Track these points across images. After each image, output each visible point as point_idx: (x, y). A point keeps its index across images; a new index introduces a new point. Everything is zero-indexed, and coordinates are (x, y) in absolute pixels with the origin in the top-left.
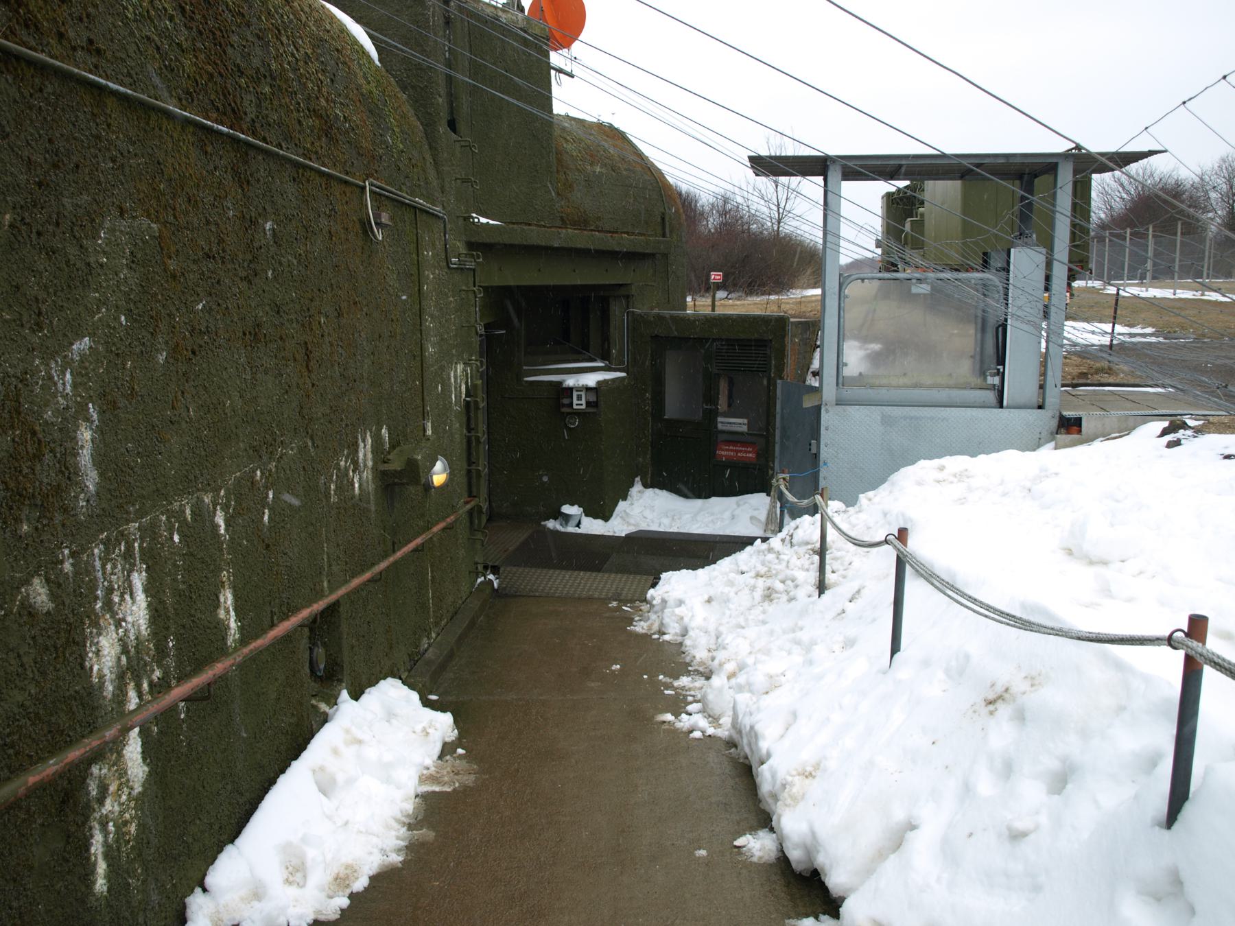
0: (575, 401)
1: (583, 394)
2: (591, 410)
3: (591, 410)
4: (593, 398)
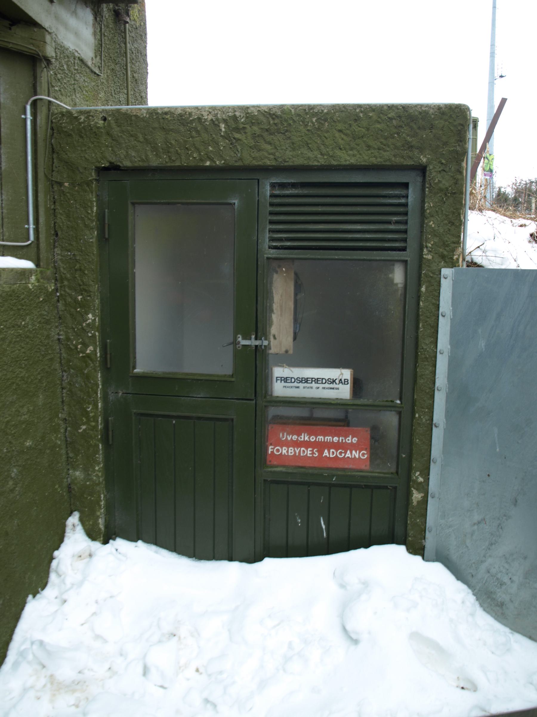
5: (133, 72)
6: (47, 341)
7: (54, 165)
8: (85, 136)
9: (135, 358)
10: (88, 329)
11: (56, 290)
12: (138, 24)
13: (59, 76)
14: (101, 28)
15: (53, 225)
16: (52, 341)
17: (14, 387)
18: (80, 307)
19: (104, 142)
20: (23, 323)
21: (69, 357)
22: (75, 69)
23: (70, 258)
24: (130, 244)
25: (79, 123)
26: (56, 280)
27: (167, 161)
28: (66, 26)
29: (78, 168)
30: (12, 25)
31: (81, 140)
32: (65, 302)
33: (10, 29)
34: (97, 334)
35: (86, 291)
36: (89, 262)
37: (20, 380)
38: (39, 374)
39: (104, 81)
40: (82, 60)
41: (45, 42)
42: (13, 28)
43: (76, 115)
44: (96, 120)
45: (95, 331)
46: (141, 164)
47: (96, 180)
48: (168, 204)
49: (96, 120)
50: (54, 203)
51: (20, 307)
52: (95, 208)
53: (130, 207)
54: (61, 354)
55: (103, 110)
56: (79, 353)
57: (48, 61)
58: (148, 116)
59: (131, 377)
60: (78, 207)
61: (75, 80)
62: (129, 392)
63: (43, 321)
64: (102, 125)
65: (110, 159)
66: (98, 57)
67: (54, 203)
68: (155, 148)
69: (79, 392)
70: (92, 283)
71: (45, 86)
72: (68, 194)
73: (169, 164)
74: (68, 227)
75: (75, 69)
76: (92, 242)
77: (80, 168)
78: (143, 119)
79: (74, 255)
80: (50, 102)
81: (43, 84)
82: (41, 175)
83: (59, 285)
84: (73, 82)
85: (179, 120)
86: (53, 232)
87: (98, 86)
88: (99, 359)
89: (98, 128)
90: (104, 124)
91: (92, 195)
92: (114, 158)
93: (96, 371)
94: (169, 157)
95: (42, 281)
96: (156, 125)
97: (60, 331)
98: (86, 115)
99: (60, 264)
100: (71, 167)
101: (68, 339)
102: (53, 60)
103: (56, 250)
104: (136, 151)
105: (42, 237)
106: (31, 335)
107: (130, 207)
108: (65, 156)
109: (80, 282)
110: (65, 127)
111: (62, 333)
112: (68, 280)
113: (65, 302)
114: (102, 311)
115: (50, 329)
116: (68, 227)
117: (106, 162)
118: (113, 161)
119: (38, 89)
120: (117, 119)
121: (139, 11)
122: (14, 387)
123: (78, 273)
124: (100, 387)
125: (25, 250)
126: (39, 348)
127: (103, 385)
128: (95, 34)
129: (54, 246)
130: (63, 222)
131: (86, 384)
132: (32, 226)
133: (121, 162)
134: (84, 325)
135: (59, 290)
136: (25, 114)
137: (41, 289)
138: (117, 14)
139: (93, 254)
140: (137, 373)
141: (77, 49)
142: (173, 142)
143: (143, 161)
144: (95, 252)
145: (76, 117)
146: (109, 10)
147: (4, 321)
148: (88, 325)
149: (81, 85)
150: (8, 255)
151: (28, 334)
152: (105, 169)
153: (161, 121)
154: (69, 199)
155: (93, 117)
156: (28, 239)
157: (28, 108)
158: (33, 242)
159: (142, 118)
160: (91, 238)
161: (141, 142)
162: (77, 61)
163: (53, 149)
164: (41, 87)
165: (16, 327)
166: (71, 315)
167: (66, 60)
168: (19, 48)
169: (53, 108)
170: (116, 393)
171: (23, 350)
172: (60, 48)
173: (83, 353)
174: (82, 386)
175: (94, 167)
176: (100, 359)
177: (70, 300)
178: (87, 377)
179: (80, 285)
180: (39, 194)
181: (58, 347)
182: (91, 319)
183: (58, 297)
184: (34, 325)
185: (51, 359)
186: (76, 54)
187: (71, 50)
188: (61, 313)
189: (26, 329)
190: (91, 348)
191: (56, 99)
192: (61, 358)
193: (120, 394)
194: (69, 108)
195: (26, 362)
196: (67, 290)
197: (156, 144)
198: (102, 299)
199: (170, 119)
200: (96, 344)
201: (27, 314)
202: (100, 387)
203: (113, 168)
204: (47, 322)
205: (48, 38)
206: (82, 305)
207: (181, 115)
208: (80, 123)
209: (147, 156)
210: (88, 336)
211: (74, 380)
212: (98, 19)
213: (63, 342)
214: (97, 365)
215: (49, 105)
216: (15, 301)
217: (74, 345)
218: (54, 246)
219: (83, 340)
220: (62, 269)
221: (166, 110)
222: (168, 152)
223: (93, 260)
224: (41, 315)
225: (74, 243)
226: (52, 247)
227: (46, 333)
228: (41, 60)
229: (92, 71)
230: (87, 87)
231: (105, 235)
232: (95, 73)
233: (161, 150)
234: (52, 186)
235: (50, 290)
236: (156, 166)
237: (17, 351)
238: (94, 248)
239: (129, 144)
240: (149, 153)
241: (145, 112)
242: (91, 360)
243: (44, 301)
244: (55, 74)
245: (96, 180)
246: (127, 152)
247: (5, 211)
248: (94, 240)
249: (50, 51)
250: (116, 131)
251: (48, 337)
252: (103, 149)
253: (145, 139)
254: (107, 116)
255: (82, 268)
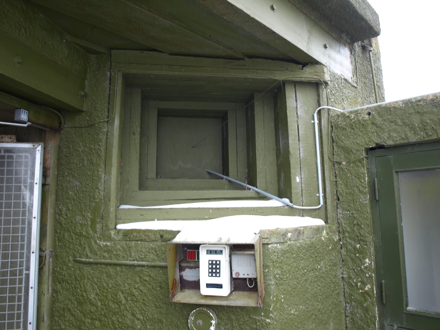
0: (205, 277)
1: (223, 259)
2: (243, 300)
3: (243, 300)
4: (244, 269)
5: (377, 82)
6: (335, 280)
7: (334, 151)
8: (355, 128)
9: (407, 297)
10: (366, 271)
11: (340, 240)
12: (376, 52)
13: (333, 92)
14: (355, 58)
15: (335, 193)
16: (338, 279)
17: (314, 317)
18: (359, 253)
19: (370, 130)
20: (319, 267)
21: (351, 292)
22: (342, 86)
23: (350, 216)
24: (397, 203)
25: (351, 119)
26: (339, 232)
27: (424, 136)
28: (334, 60)
29: (352, 151)
30: (303, 67)
31: (353, 131)
32: (347, 249)
33: (302, 69)
34: (373, 275)
35: (363, 240)
36: (365, 219)
37: (317, 312)
38: (330, 305)
39: (360, 91)
40: (346, 80)
41: (324, 72)
42: (304, 68)
43: (348, 115)
44: (363, 116)
45: (371, 273)
46: (402, 142)
47: (366, 158)
48: (428, 169)
49: (363, 116)
50: (336, 177)
51: (317, 255)
52: (367, 178)
53: (395, 174)
54: (344, 289)
55: (368, 108)
56: (358, 289)
57: (326, 83)
58: (404, 105)
59: (405, 313)
60: (353, 178)
61: (343, 93)
62: (404, 326)
63: (332, 264)
64: (368, 118)
65: (376, 141)
66: (355, 76)
67: (336, 177)
68: (412, 128)
69: (360, 321)
70: (367, 235)
71: (325, 100)
72: (345, 170)
73: (426, 139)
74: (346, 193)
75: (342, 86)
76: (366, 203)
77: (353, 151)
78: (400, 109)
79: (352, 213)
80: (329, 110)
81: (324, 99)
82: (326, 158)
83: (341, 236)
84: (342, 94)
85: (431, 104)
86: (336, 198)
87: (357, 95)
88: (375, 296)
89: (365, 121)
90: (369, 117)
91: (364, 169)
92: (379, 140)
93: (373, 305)
94: (426, 133)
95: (330, 234)
96: (412, 111)
97: (343, 271)
98: (355, 114)
99: (342, 220)
100: (347, 151)
101: (350, 278)
102: (329, 83)
103: (338, 210)
104: (396, 133)
105: (329, 201)
106: (324, 276)
107: (395, 174)
108: (342, 144)
109: (358, 234)
110: (340, 124)
111: (345, 272)
112: (348, 232)
113: (347, 249)
114: (376, 257)
115: (336, 270)
116: (346, 193)
117: (373, 143)
118: (378, 142)
119: (321, 102)
120: (379, 112)
121: (376, 44)
122: (314, 317)
123: (356, 227)
124: (377, 319)
125: (317, 211)
126: (330, 286)
127: (379, 318)
128: (351, 62)
129: (337, 207)
130: (343, 190)
131: (365, 316)
132: (321, 195)
133: (385, 142)
134: (363, 267)
135: (341, 240)
136: (314, 120)
137: (330, 240)
138: (364, 48)
139: (367, 213)
140: (410, 311)
141: (342, 74)
142: (428, 121)
143: (403, 139)
144: (369, 211)
145: (348, 116)
146: (359, 46)
147: (307, 266)
148: (366, 267)
149: (346, 95)
150: (306, 216)
151: (322, 275)
152: (372, 149)
153: (416, 107)
154: (346, 173)
155: (360, 114)
156: (319, 204)
157: (316, 115)
158: (322, 206)
159: (399, 108)
160: (366, 201)
161: (400, 126)
162: (343, 81)
163: (333, 140)
164: (323, 101)
165: (314, 270)
166: (351, 259)
167: (337, 81)
168: (308, 79)
169: (331, 113)
170: (392, 326)
171: (319, 287)
172: (333, 75)
173: (362, 290)
174: (362, 316)
175: (364, 149)
176: (377, 295)
177: (350, 247)
178: (366, 310)
179: (358, 236)
180: (325, 172)
181: (342, 284)
182: (369, 263)
183: (341, 245)
184: (326, 268)
185: (338, 294)
186: (342, 77)
187: (339, 74)
188: (343, 257)
189: (321, 271)
190: (369, 286)
191: (333, 106)
192: (344, 292)
193: (396, 327)
194: (342, 111)
195: (321, 297)
196: (348, 239)
197: (414, 125)
198: (375, 248)
199: (423, 104)
200: (373, 283)
201: (321, 260)
202: (377, 319)
203: (380, 147)
204: (335, 265)
205: (325, 70)
206: (360, 251)
207: (432, 100)
208: (351, 120)
209: (406, 135)
210: (366, 276)
211: (355, 311)
212: (353, 53)
213: (346, 280)
214: (375, 300)
215: (328, 111)
216: (313, 251)
217: (354, 283)
218: (337, 207)
219: (361, 279)
220: (343, 224)
221: (419, 98)
222: (425, 130)
223: (367, 217)
224: (331, 260)
225: (352, 205)
226: (336, 208)
227: (334, 273)
228: (322, 84)
229: (352, 86)
230: (350, 96)
231: (375, 197)
232: (354, 87)
233: (418, 129)
234: (334, 165)
235: (336, 240)
236: (415, 142)
237: (316, 289)
238: (368, 208)
239: (390, 128)
240: (408, 133)
241: (401, 103)
242: (369, 296)
243: (333, 249)
244: (331, 91)
245: (366, 158)
246: (389, 135)
247: (303, 185)
248: (367, 202)
249: (327, 77)
250: (379, 120)
251: (335, 276)
252: (370, 135)
253: (403, 122)
254: (371, 112)
255: (359, 223)
